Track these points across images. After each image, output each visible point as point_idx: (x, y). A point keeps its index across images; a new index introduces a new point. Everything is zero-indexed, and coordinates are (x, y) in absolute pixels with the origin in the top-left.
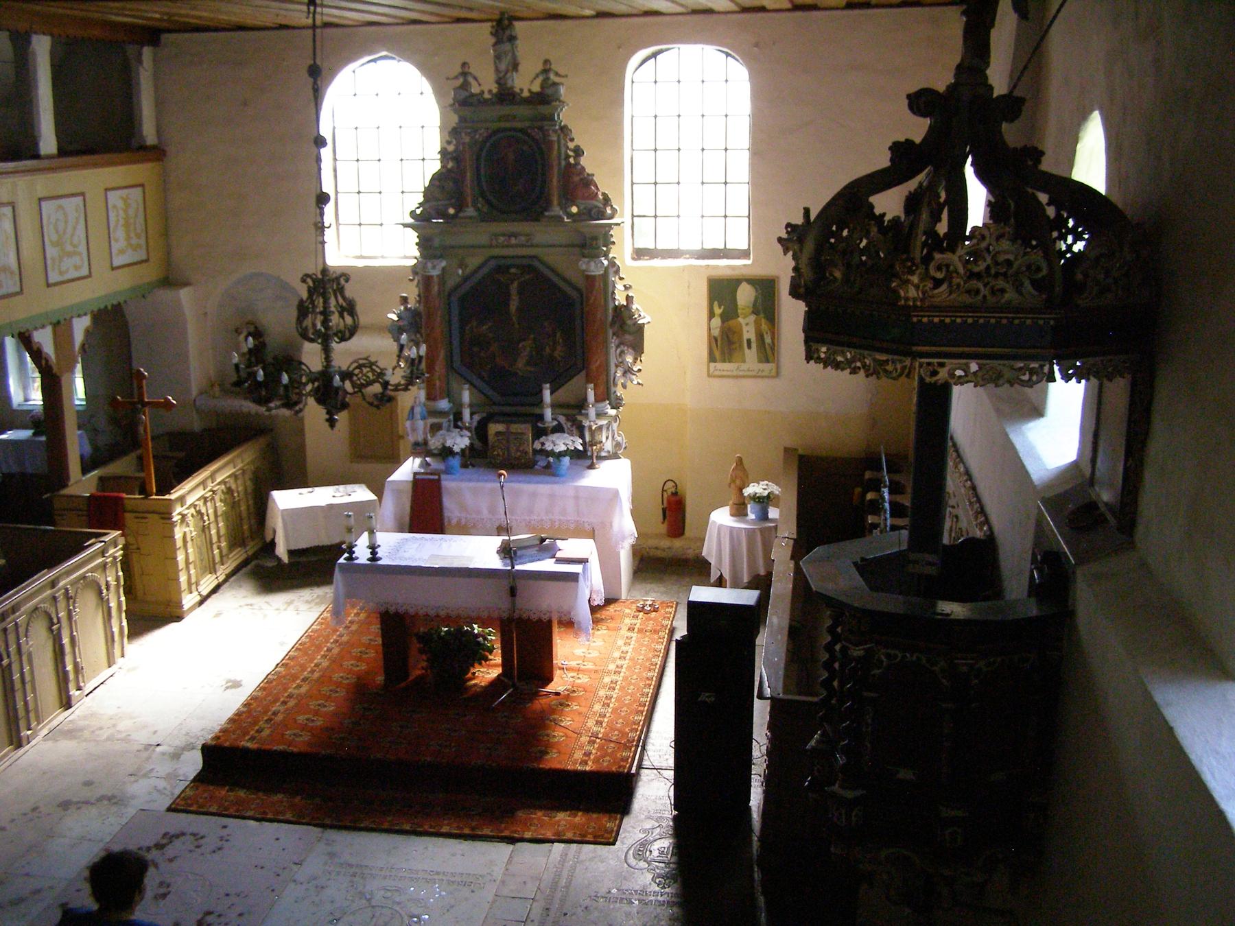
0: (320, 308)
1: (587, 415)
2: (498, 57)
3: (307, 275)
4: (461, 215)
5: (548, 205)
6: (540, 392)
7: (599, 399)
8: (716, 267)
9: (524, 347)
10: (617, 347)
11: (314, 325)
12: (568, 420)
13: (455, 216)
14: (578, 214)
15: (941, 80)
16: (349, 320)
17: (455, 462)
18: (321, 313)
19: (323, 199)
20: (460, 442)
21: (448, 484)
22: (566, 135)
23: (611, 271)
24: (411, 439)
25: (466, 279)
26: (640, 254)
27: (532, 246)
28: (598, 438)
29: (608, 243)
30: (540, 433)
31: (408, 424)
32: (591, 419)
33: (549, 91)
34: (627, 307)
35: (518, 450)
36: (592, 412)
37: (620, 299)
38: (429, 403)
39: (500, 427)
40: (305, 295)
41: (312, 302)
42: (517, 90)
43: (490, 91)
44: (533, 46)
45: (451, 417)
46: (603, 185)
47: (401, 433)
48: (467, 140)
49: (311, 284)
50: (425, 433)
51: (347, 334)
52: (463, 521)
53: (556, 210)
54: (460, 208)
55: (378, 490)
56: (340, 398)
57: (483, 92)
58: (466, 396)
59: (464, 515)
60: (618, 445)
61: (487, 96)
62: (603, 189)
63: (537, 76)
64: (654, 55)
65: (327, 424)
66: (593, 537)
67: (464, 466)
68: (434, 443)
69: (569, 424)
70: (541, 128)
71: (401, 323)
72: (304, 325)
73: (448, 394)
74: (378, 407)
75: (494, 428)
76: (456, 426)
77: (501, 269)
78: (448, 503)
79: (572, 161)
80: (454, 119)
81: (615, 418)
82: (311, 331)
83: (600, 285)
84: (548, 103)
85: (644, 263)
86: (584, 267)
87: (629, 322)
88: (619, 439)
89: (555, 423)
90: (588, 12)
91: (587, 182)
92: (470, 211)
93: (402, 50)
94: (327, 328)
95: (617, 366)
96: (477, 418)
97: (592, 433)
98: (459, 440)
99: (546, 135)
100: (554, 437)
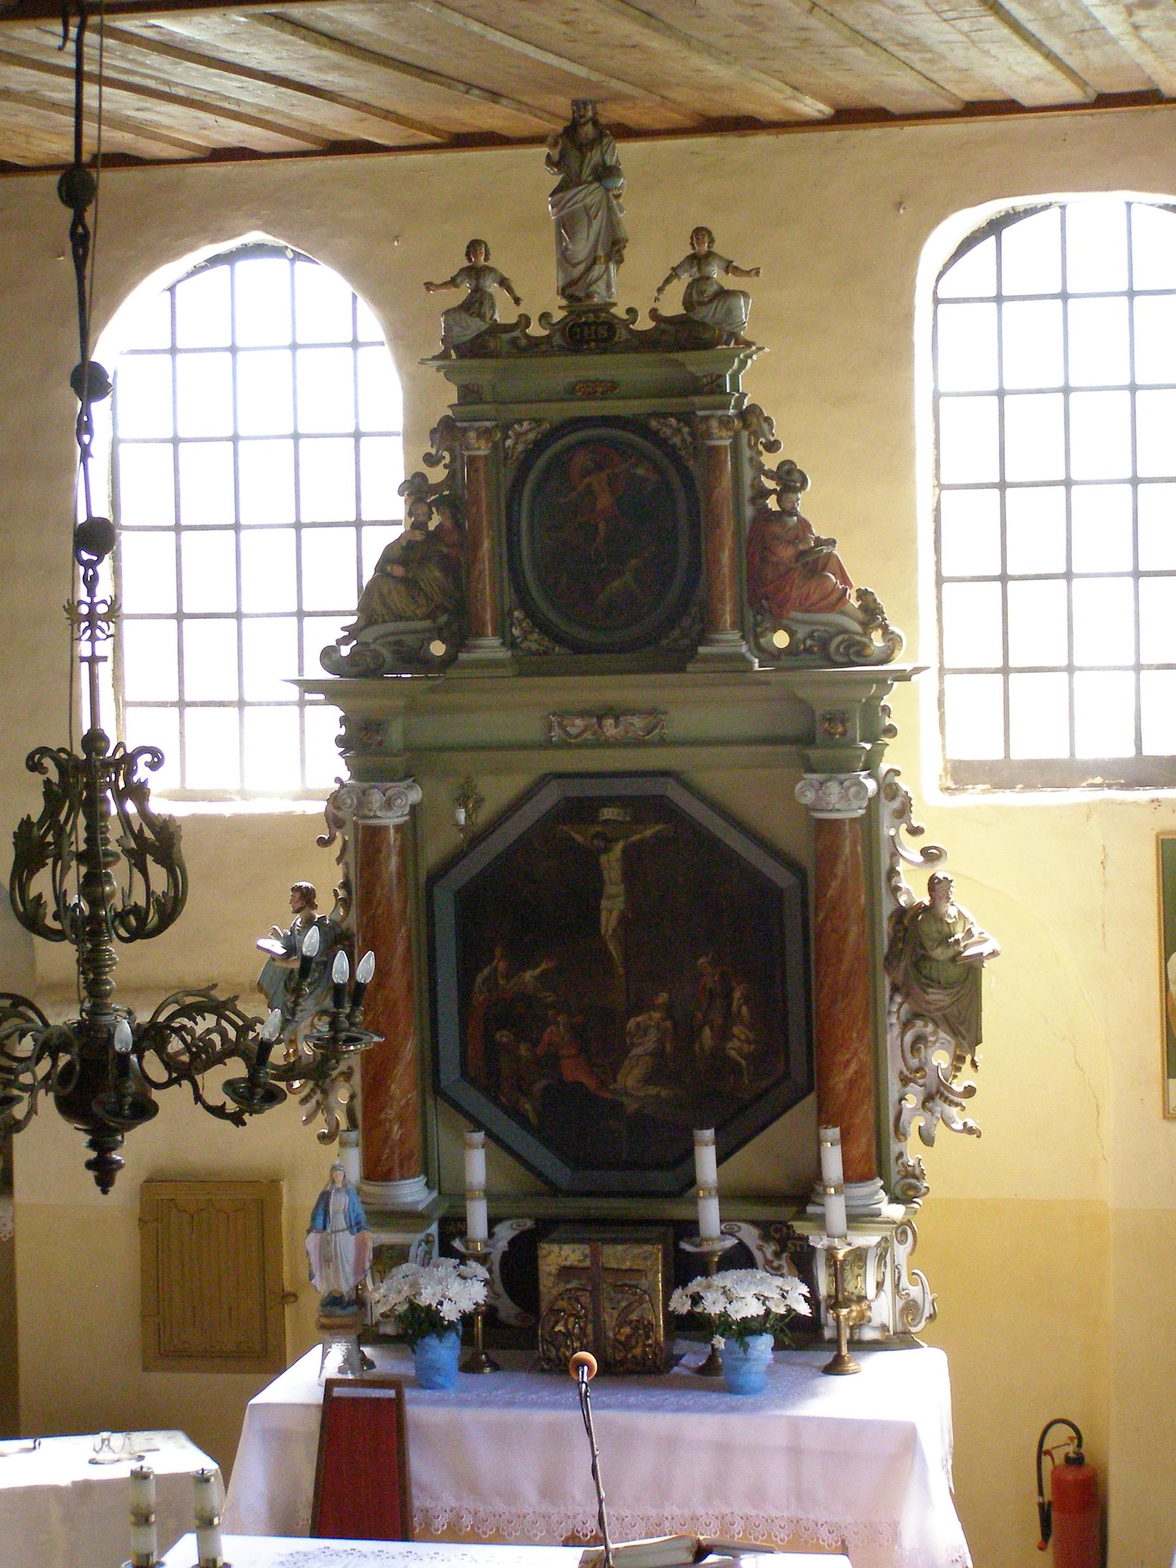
0: (79, 842)
1: (820, 1221)
2: (567, 225)
3: (43, 751)
4: (463, 656)
5: (706, 628)
6: (688, 1155)
7: (853, 1175)
9: (642, 1030)
10: (906, 1025)
11: (60, 897)
12: (766, 1237)
13: (448, 661)
14: (790, 651)
16: (158, 875)
17: (445, 1352)
18: (81, 857)
19: (97, 538)
20: (460, 1292)
21: (424, 1413)
22: (756, 434)
23: (887, 809)
24: (321, 1286)
25: (476, 839)
26: (963, 774)
27: (662, 743)
28: (851, 1286)
29: (879, 731)
30: (685, 1268)
31: (312, 1242)
32: (833, 1228)
33: (705, 314)
34: (931, 911)
35: (622, 1322)
36: (836, 1208)
37: (913, 888)
38: (372, 1189)
40: (36, 808)
41: (60, 831)
42: (619, 312)
43: (545, 317)
44: (660, 198)
45: (434, 1229)
46: (861, 569)
47: (288, 1288)
48: (482, 449)
49: (54, 775)
50: (359, 1269)
51: (153, 919)
53: (730, 640)
54: (459, 640)
55: (220, 1442)
56: (132, 1086)
57: (525, 320)
58: (477, 1166)
59: (469, 1503)
60: (910, 1309)
61: (536, 330)
62: (858, 581)
63: (675, 273)
64: (995, 227)
65: (91, 1175)
66: (844, 1551)
67: (470, 1366)
68: (386, 1296)
69: (770, 1249)
70: (686, 418)
72: (33, 892)
73: (425, 1165)
74: (237, 1119)
75: (557, 1256)
76: (447, 1251)
77: (579, 810)
78: (423, 1468)
79: (772, 503)
80: (445, 397)
81: (902, 1229)
82: (51, 907)
83: (849, 851)
84: (708, 345)
85: (976, 797)
86: (809, 797)
87: (939, 953)
88: (915, 1292)
89: (730, 1242)
90: (811, 107)
91: (817, 561)
92: (490, 647)
93: (307, 228)
94: (97, 901)
95: (905, 1081)
96: (506, 1233)
97: (837, 1269)
98: (455, 1288)
99: (699, 435)
100: (729, 1279)
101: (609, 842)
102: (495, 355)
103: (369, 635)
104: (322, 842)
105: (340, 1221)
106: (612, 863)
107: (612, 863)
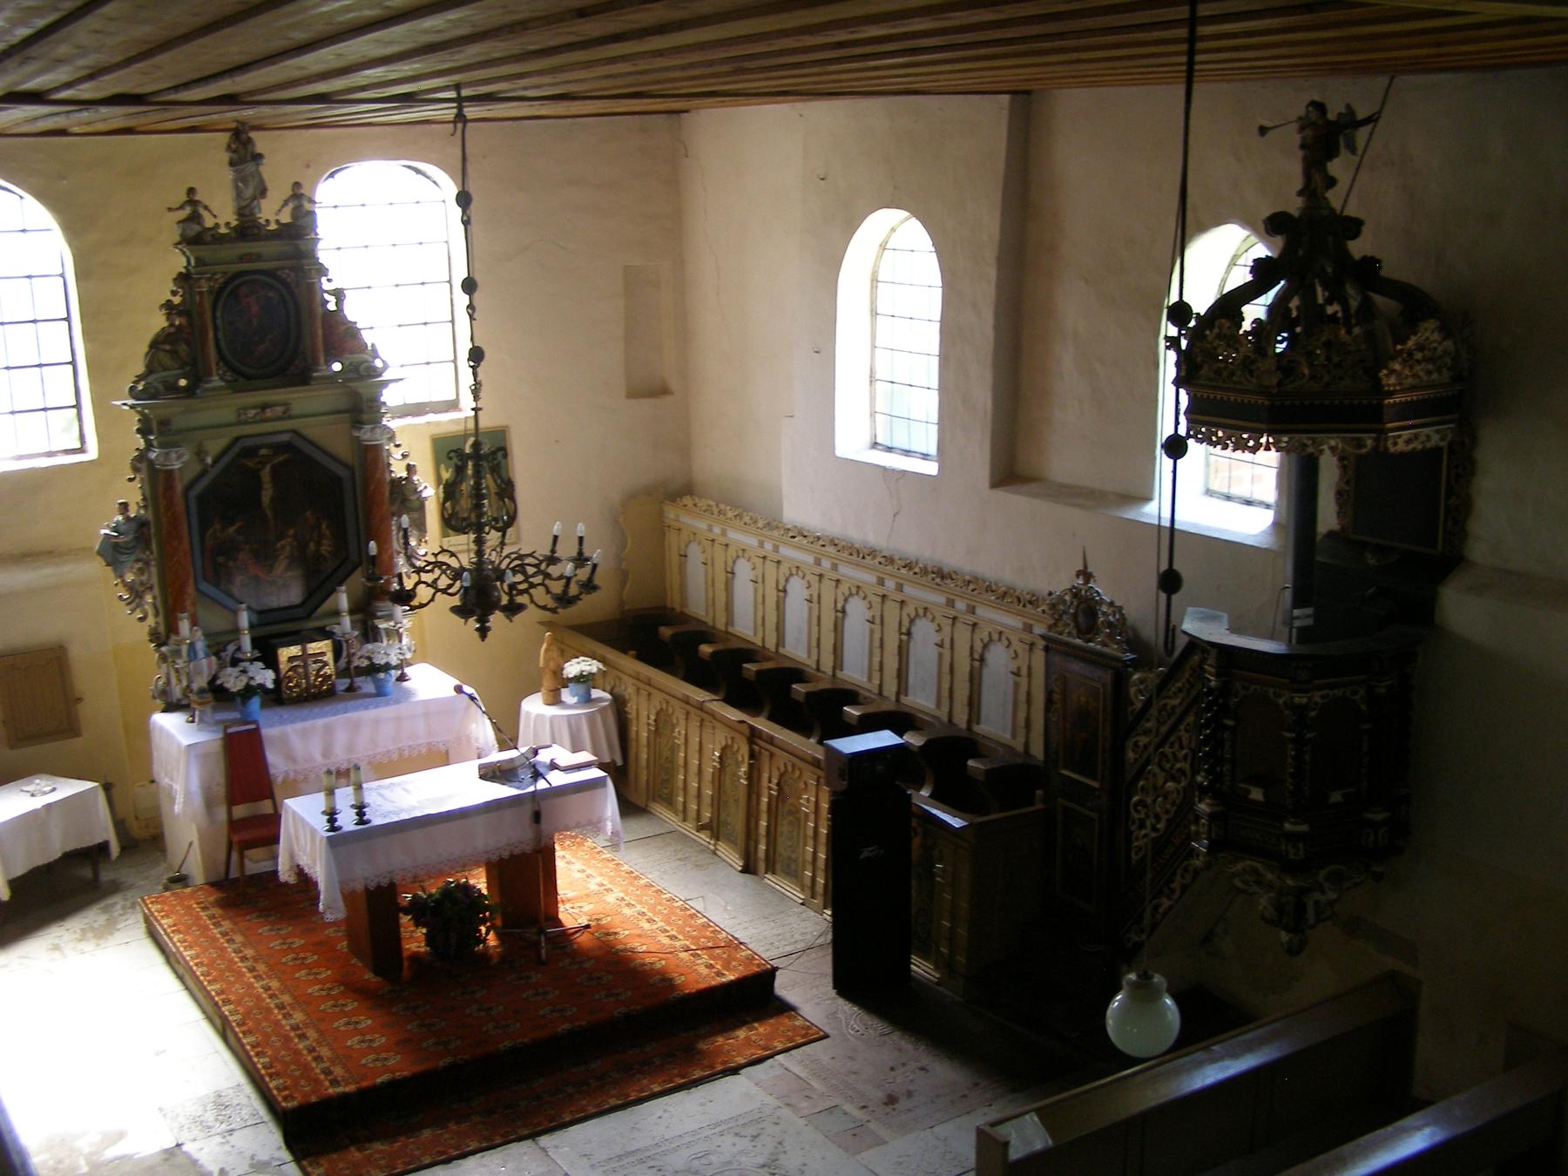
8: (438, 424)
9: (283, 547)
15: (1294, 205)
27: (290, 418)
35: (318, 676)
37: (399, 470)
39: (295, 650)
52: (292, 775)
61: (223, 230)
63: (286, 203)
71: (122, 539)
78: (276, 761)
87: (414, 498)
91: (352, 332)
92: (216, 381)
101: (263, 464)
102: (205, 244)
103: (151, 379)
104: (130, 480)
105: (201, 654)
106: (266, 474)
107: (266, 474)
